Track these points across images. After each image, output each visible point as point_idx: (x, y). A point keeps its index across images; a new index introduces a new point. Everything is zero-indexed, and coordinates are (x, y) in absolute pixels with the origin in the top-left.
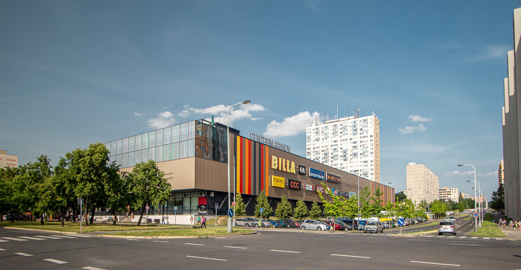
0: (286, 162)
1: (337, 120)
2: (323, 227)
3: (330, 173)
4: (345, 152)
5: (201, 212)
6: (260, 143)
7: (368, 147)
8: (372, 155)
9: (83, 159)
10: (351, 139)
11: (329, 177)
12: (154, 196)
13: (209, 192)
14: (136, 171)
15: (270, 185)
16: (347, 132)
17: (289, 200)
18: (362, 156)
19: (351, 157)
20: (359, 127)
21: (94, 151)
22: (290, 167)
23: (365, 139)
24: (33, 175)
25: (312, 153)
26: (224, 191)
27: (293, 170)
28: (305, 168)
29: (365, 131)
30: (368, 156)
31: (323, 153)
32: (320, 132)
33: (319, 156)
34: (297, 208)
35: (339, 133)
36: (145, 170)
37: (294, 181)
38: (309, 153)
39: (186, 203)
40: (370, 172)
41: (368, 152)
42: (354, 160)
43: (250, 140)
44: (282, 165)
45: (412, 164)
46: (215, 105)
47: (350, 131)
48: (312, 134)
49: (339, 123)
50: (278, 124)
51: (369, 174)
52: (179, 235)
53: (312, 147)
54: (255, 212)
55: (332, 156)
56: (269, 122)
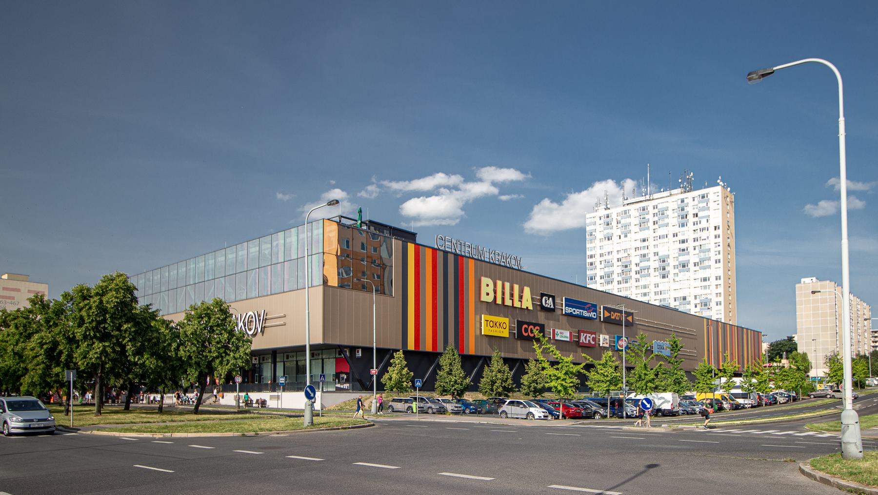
0: (512, 289)
1: (648, 197)
2: (538, 412)
3: (609, 306)
4: (664, 261)
5: (338, 385)
6: (456, 255)
7: (709, 250)
8: (718, 265)
9: (86, 302)
10: (675, 235)
11: (607, 314)
12: (217, 361)
13: (353, 349)
14: (189, 318)
15: (478, 333)
16: (666, 221)
17: (506, 360)
18: (697, 268)
19: (676, 271)
20: (690, 210)
21: (107, 287)
22: (521, 297)
23: (704, 235)
24: (21, 328)
25: (597, 264)
26: (368, 345)
27: (527, 303)
28: (553, 297)
29: (703, 217)
30: (709, 267)
31: (620, 263)
32: (614, 223)
33: (611, 269)
34: (525, 377)
35: (651, 224)
36: (200, 317)
37: (529, 324)
38: (591, 264)
39: (267, 373)
40: (715, 299)
41: (709, 259)
42: (681, 276)
43: (435, 250)
44: (503, 294)
45: (807, 280)
46: (430, 173)
47: (673, 219)
48: (597, 227)
49: (651, 204)
50: (555, 205)
51: (713, 305)
52: (210, 432)
53: (598, 252)
54: (437, 384)
55: (638, 269)
56: (538, 202)
